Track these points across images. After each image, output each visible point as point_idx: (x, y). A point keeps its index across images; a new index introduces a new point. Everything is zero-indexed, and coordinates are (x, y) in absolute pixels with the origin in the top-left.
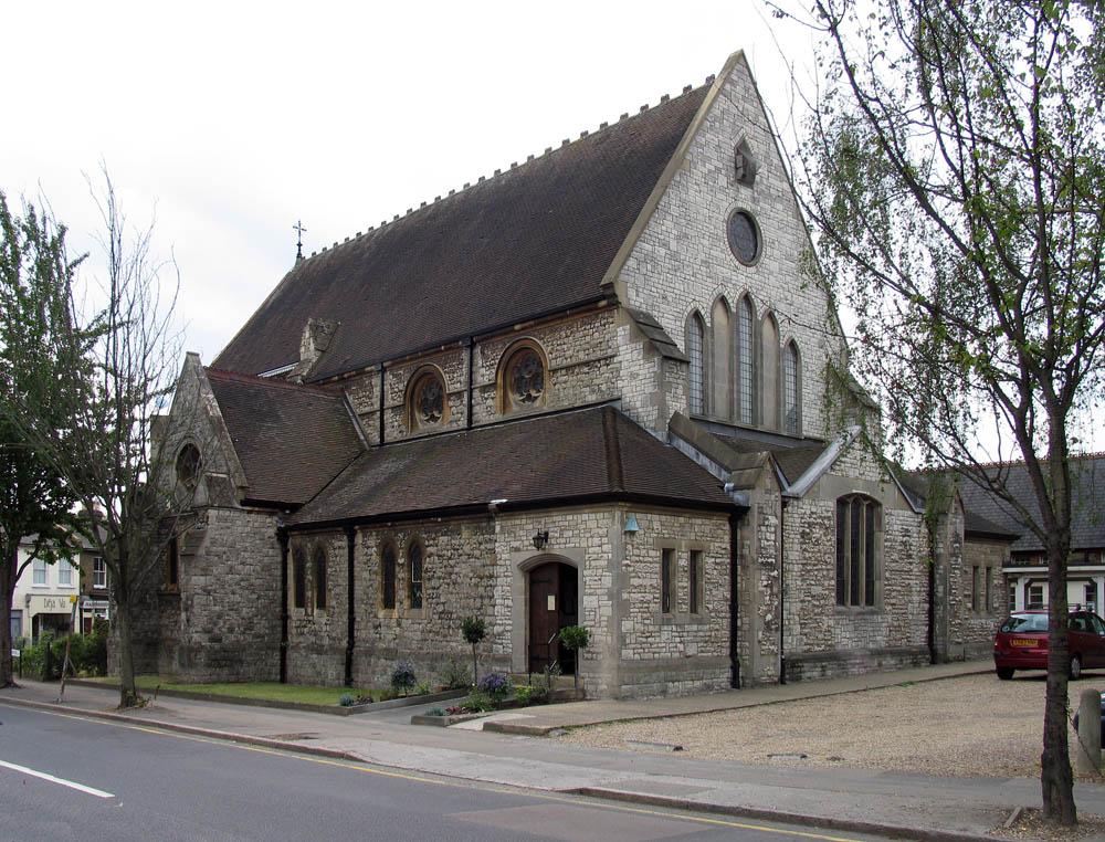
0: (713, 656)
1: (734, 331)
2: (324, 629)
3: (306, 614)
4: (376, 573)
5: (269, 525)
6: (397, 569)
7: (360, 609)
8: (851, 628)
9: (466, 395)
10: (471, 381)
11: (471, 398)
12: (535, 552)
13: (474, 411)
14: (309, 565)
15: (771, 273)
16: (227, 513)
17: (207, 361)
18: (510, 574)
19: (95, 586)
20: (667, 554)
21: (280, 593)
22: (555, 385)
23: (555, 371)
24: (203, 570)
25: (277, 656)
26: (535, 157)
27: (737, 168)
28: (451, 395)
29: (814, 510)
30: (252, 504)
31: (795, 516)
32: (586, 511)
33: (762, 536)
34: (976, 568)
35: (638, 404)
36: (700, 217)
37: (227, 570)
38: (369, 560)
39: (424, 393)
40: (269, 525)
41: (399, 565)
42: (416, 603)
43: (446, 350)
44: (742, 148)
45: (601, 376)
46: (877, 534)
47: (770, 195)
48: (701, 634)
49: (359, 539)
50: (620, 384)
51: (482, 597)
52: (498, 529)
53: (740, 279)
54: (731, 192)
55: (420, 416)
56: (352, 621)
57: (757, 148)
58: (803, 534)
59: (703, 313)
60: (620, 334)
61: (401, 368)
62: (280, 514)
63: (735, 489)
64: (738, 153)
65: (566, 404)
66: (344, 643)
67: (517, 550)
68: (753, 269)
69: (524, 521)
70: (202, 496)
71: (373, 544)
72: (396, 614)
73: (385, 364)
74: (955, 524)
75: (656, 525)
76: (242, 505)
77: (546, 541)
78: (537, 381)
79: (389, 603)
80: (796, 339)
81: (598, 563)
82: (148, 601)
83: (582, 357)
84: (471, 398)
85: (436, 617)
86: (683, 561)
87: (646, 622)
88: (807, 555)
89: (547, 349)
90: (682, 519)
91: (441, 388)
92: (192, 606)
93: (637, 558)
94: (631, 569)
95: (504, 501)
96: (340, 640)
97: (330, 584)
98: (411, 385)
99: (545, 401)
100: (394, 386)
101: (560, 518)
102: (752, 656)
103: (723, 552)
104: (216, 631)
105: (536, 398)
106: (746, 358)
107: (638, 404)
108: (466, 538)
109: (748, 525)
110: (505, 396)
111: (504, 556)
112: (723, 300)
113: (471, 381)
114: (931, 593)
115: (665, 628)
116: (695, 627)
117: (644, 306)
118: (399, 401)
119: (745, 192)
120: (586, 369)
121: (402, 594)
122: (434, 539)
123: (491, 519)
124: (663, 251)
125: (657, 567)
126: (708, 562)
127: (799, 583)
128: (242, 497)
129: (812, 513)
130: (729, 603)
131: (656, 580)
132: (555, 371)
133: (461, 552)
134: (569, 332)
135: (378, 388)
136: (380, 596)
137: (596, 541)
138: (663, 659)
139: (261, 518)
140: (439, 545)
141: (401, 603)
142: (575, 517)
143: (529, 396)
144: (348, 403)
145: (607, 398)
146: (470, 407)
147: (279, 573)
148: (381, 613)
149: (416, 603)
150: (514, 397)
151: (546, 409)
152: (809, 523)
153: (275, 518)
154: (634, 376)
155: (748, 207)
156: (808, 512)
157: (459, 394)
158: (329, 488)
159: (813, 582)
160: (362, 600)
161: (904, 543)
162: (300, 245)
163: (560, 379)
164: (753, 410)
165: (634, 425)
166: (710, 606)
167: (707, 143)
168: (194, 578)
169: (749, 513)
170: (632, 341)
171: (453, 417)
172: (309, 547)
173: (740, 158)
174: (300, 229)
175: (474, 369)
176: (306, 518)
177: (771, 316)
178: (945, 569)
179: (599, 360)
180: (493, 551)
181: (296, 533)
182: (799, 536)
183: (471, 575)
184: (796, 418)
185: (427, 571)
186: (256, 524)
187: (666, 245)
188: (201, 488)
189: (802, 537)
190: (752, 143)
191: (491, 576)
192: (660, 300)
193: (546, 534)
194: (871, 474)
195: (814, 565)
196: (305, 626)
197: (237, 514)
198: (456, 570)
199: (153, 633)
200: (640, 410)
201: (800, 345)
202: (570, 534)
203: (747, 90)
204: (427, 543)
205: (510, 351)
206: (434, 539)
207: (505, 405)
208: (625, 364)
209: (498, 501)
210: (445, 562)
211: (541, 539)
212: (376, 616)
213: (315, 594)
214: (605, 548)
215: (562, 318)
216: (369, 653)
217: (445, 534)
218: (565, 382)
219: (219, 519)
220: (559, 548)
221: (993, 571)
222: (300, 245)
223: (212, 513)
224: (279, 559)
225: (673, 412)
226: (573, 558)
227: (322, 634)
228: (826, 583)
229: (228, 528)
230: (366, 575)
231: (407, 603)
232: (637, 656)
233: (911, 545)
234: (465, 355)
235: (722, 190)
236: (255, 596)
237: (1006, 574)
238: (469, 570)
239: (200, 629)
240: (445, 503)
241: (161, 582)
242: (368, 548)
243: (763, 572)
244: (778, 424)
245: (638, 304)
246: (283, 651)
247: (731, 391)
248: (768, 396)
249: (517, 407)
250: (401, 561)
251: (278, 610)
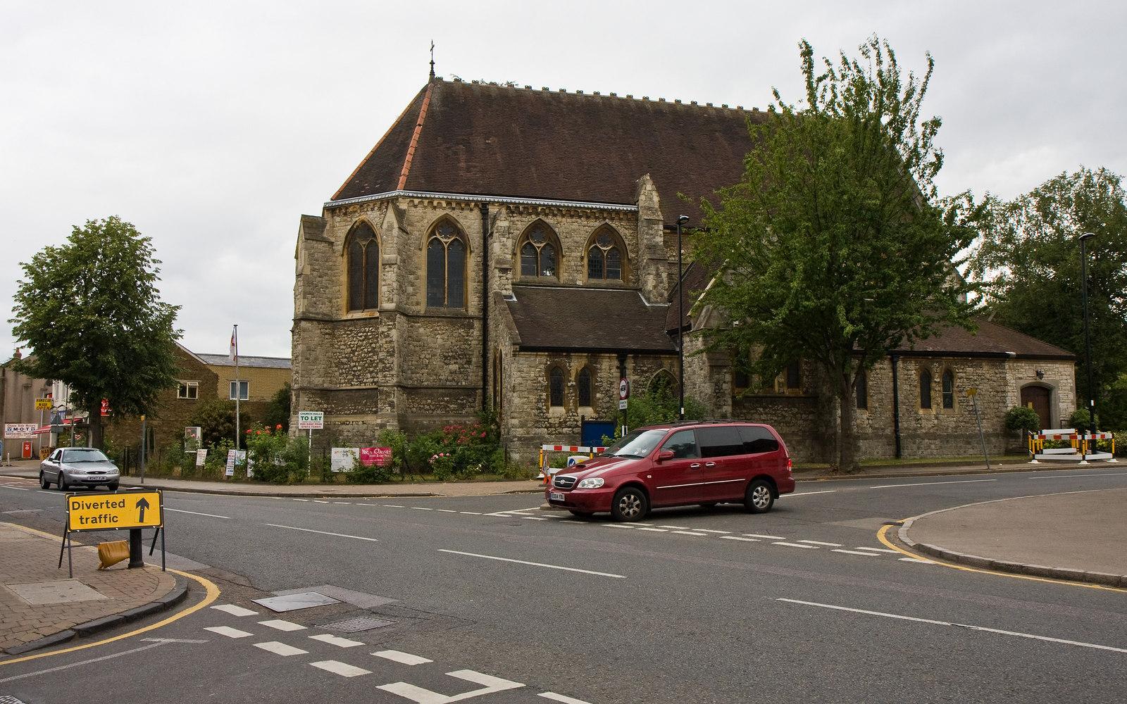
2: (867, 422)
7: (902, 409)
26: (729, 107)
41: (936, 382)
42: (948, 403)
49: (900, 364)
51: (999, 402)
52: (1007, 367)
56: (896, 415)
66: (889, 431)
67: (1021, 378)
69: (1023, 365)
71: (913, 368)
85: (967, 413)
101: (1044, 365)
108: (986, 370)
122: (963, 369)
123: (1004, 362)
140: (965, 373)
148: (921, 412)
149: (948, 403)
162: (432, 63)
178: (118, 384)
198: (980, 387)
206: (963, 369)
210: (973, 383)
216: (914, 436)
217: (972, 367)
222: (432, 63)
230: (906, 387)
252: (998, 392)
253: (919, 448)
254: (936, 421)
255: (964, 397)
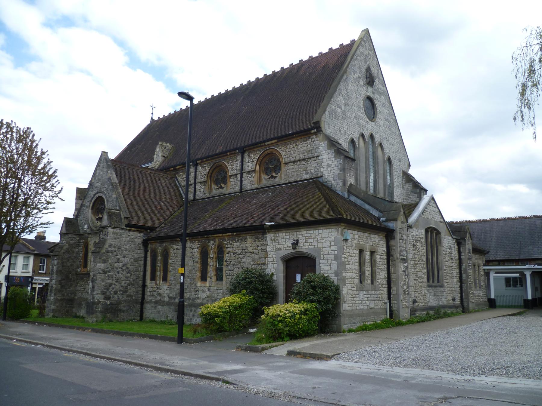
0: (381, 308)
1: (367, 150)
2: (166, 292)
3: (156, 285)
4: (197, 262)
5: (138, 237)
6: (209, 260)
8: (433, 293)
9: (239, 176)
10: (242, 169)
11: (242, 177)
12: (290, 250)
13: (243, 183)
14: (159, 258)
15: (380, 126)
16: (118, 231)
17: (113, 156)
18: (275, 262)
19: (40, 272)
20: (361, 252)
21: (142, 274)
22: (287, 170)
23: (287, 164)
24: (103, 260)
25: (138, 306)
27: (367, 78)
28: (231, 176)
29: (417, 234)
30: (131, 226)
31: (410, 236)
32: (322, 228)
33: (398, 244)
34: (474, 266)
35: (332, 179)
36: (353, 97)
37: (116, 260)
38: (194, 255)
39: (217, 176)
40: (138, 237)
41: (211, 258)
43: (230, 154)
44: (368, 70)
45: (312, 165)
46: (439, 248)
47: (379, 92)
48: (376, 296)
49: (188, 244)
50: (322, 169)
52: (268, 239)
53: (369, 127)
54: (365, 88)
55: (214, 186)
57: (374, 71)
58: (414, 245)
59: (355, 140)
60: (322, 146)
61: (205, 164)
62: (145, 232)
63: (387, 220)
64: (367, 71)
65: (293, 179)
67: (280, 249)
68: (373, 123)
69: (284, 234)
70: (105, 222)
71: (196, 247)
72: (207, 284)
73: (198, 162)
74: (469, 245)
75: (356, 237)
76: (126, 227)
77: (298, 245)
78: (277, 169)
79: (204, 278)
80: (391, 157)
81: (329, 256)
82: (70, 277)
83: (302, 156)
84: (242, 177)
86: (367, 257)
87: (353, 289)
88: (416, 256)
89: (283, 154)
90: (367, 235)
91: (226, 173)
92: (96, 280)
93: (349, 254)
94: (346, 260)
95: (273, 223)
96: (175, 298)
97: (170, 268)
98: (211, 171)
99: (281, 178)
100: (203, 171)
101: (305, 232)
102: (398, 308)
103: (383, 252)
104: (108, 293)
105: (276, 177)
106: (371, 163)
107: (332, 179)
109: (394, 239)
110: (260, 176)
111: (272, 253)
112: (363, 135)
113: (242, 169)
114: (461, 278)
115: (361, 292)
116: (373, 292)
117: (332, 134)
118: (204, 179)
119: (370, 89)
120: (303, 163)
121: (211, 272)
123: (265, 233)
124: (339, 110)
125: (357, 259)
126: (378, 258)
127: (413, 270)
128: (127, 223)
129: (416, 235)
130: (387, 280)
131: (357, 267)
132: (287, 164)
133: (246, 251)
134: (294, 145)
135: (194, 173)
136: (199, 274)
137: (328, 244)
138: (360, 309)
139: (135, 234)
141: (211, 278)
142: (315, 231)
143: (272, 177)
144: (177, 180)
145: (314, 176)
146: (241, 181)
147: (142, 262)
148: (199, 284)
149: (220, 278)
150: (264, 176)
151: (282, 182)
152: (415, 240)
153: (142, 234)
154: (329, 166)
155: (371, 95)
156: (415, 235)
157: (236, 175)
158: (169, 220)
159: (418, 270)
160: (188, 277)
161: (449, 253)
163: (289, 167)
164: (375, 187)
165: (330, 189)
166: (379, 281)
167: (355, 65)
168: (98, 264)
169: (395, 232)
170: (328, 149)
171: (232, 186)
172: (160, 249)
173: (368, 74)
174: (153, 107)
175: (244, 163)
176: (156, 234)
177: (381, 145)
178: (465, 266)
179: (310, 158)
180: (265, 251)
181: (153, 242)
182: (412, 246)
183: (252, 263)
184: (391, 194)
185: (226, 261)
186: (132, 237)
187: (340, 107)
188: (105, 217)
189: (413, 247)
190: (372, 68)
191: (264, 264)
192: (338, 132)
193: (297, 241)
194: (437, 218)
195: (418, 261)
196: (155, 291)
197: (123, 231)
198: (244, 260)
199: (71, 294)
200: (333, 182)
201: (392, 160)
202: (311, 240)
203: (370, 45)
204: (227, 246)
205: (264, 155)
206: (231, 244)
207: (260, 180)
208: (324, 160)
209: (270, 224)
210: (237, 257)
211: (296, 244)
212: (196, 286)
213: (162, 274)
214: (333, 248)
215: (290, 139)
217: (238, 241)
218: (292, 169)
219: (114, 234)
220: (304, 247)
221: (480, 268)
222: (152, 114)
223: (110, 230)
224: (143, 255)
225: (349, 183)
226: (314, 254)
227: (165, 295)
228: (423, 271)
229: (118, 238)
230: (191, 263)
231: (214, 278)
232: (349, 308)
233: (452, 254)
234: (239, 157)
235: (362, 86)
236: (129, 275)
237: (484, 269)
238: (251, 260)
239: (100, 293)
240: (239, 224)
241: (78, 267)
242: (193, 249)
243: (402, 264)
244: (385, 194)
245: (329, 132)
246: (142, 304)
247: (366, 177)
248: (381, 181)
249: (266, 181)
250: (211, 256)
251: (140, 282)
252: (258, 265)
253: (193, 316)
254: (208, 293)
255: (230, 270)
